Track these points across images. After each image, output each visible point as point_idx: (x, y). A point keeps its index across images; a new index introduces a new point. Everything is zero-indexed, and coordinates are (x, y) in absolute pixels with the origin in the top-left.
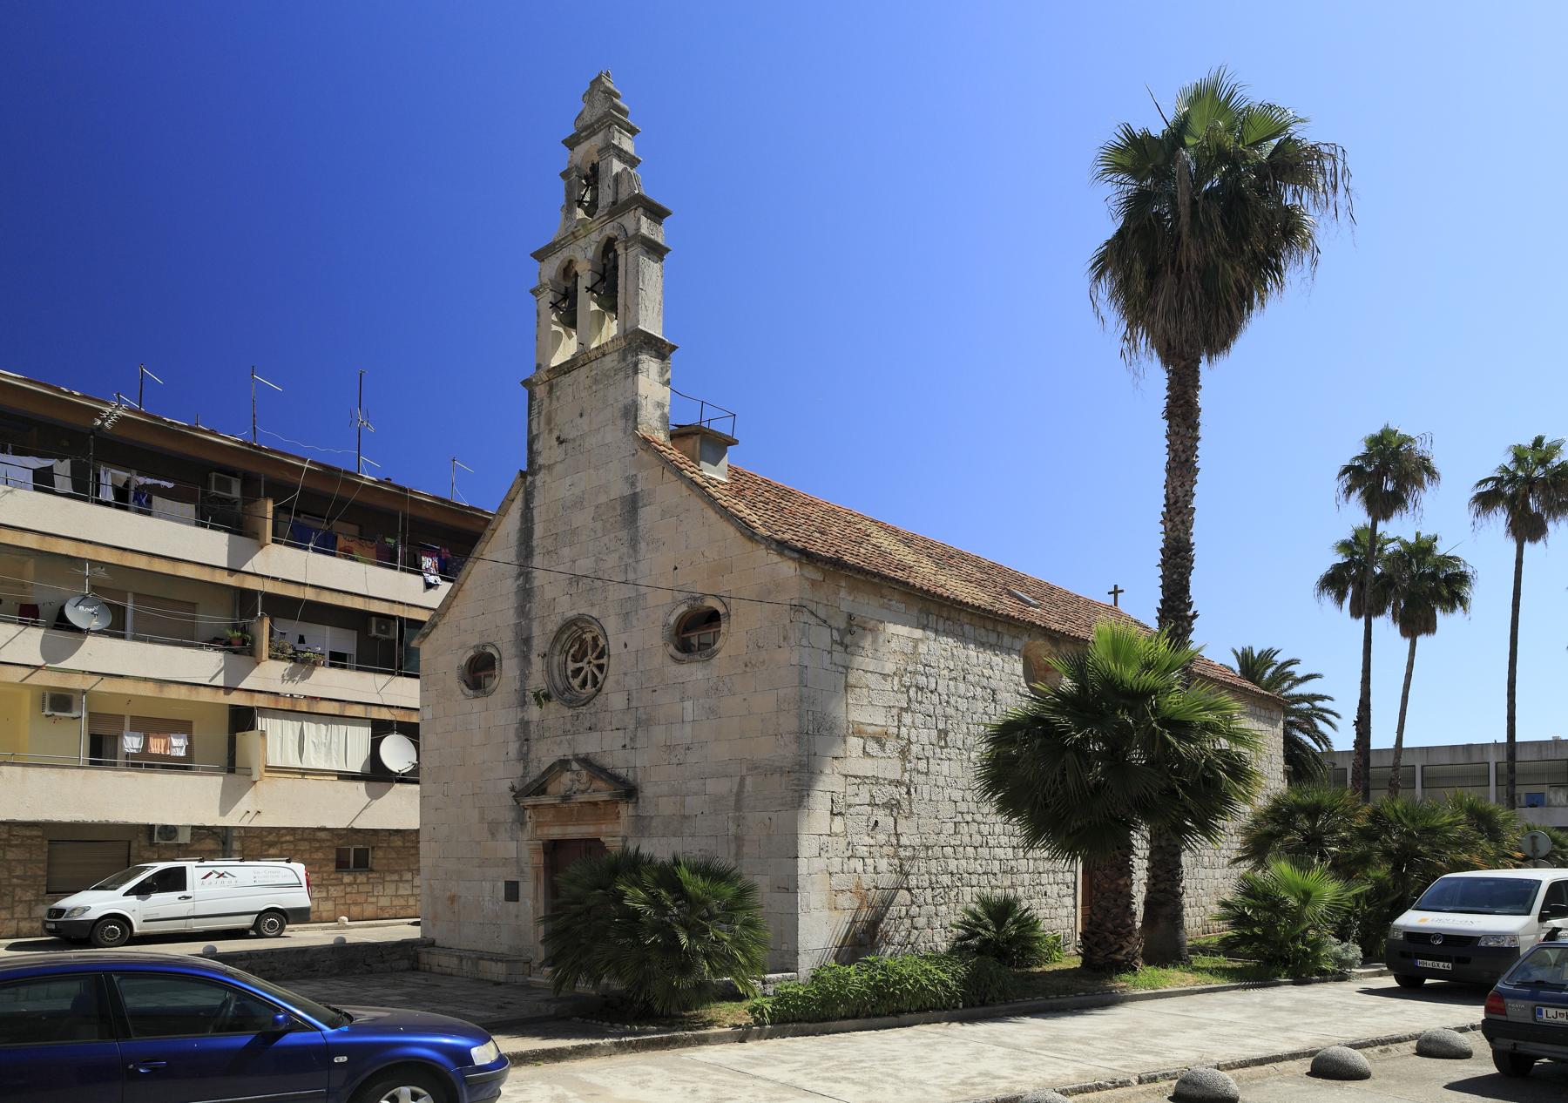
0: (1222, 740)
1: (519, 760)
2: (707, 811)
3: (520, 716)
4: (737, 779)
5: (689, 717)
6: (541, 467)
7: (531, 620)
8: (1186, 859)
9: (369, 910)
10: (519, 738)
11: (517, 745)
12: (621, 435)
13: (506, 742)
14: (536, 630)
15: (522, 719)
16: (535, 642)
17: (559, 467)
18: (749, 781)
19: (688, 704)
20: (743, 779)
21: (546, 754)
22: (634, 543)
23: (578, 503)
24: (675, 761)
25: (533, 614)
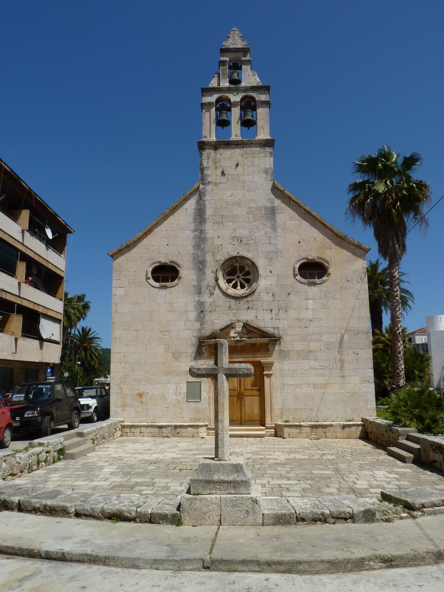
0: (381, 347)
1: (197, 321)
2: (323, 348)
3: (197, 299)
4: (339, 335)
5: (310, 307)
6: (209, 183)
7: (205, 253)
8: (210, 379)
9: (190, 567)
10: (197, 310)
11: (195, 313)
12: (264, 180)
13: (186, 311)
14: (209, 258)
15: (198, 302)
16: (208, 264)
17: (221, 186)
18: (346, 337)
19: (310, 302)
20: (342, 337)
21: (216, 321)
22: (274, 228)
23: (238, 204)
24: (304, 325)
25: (206, 250)
